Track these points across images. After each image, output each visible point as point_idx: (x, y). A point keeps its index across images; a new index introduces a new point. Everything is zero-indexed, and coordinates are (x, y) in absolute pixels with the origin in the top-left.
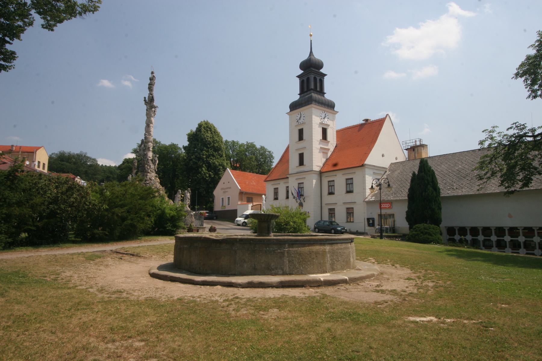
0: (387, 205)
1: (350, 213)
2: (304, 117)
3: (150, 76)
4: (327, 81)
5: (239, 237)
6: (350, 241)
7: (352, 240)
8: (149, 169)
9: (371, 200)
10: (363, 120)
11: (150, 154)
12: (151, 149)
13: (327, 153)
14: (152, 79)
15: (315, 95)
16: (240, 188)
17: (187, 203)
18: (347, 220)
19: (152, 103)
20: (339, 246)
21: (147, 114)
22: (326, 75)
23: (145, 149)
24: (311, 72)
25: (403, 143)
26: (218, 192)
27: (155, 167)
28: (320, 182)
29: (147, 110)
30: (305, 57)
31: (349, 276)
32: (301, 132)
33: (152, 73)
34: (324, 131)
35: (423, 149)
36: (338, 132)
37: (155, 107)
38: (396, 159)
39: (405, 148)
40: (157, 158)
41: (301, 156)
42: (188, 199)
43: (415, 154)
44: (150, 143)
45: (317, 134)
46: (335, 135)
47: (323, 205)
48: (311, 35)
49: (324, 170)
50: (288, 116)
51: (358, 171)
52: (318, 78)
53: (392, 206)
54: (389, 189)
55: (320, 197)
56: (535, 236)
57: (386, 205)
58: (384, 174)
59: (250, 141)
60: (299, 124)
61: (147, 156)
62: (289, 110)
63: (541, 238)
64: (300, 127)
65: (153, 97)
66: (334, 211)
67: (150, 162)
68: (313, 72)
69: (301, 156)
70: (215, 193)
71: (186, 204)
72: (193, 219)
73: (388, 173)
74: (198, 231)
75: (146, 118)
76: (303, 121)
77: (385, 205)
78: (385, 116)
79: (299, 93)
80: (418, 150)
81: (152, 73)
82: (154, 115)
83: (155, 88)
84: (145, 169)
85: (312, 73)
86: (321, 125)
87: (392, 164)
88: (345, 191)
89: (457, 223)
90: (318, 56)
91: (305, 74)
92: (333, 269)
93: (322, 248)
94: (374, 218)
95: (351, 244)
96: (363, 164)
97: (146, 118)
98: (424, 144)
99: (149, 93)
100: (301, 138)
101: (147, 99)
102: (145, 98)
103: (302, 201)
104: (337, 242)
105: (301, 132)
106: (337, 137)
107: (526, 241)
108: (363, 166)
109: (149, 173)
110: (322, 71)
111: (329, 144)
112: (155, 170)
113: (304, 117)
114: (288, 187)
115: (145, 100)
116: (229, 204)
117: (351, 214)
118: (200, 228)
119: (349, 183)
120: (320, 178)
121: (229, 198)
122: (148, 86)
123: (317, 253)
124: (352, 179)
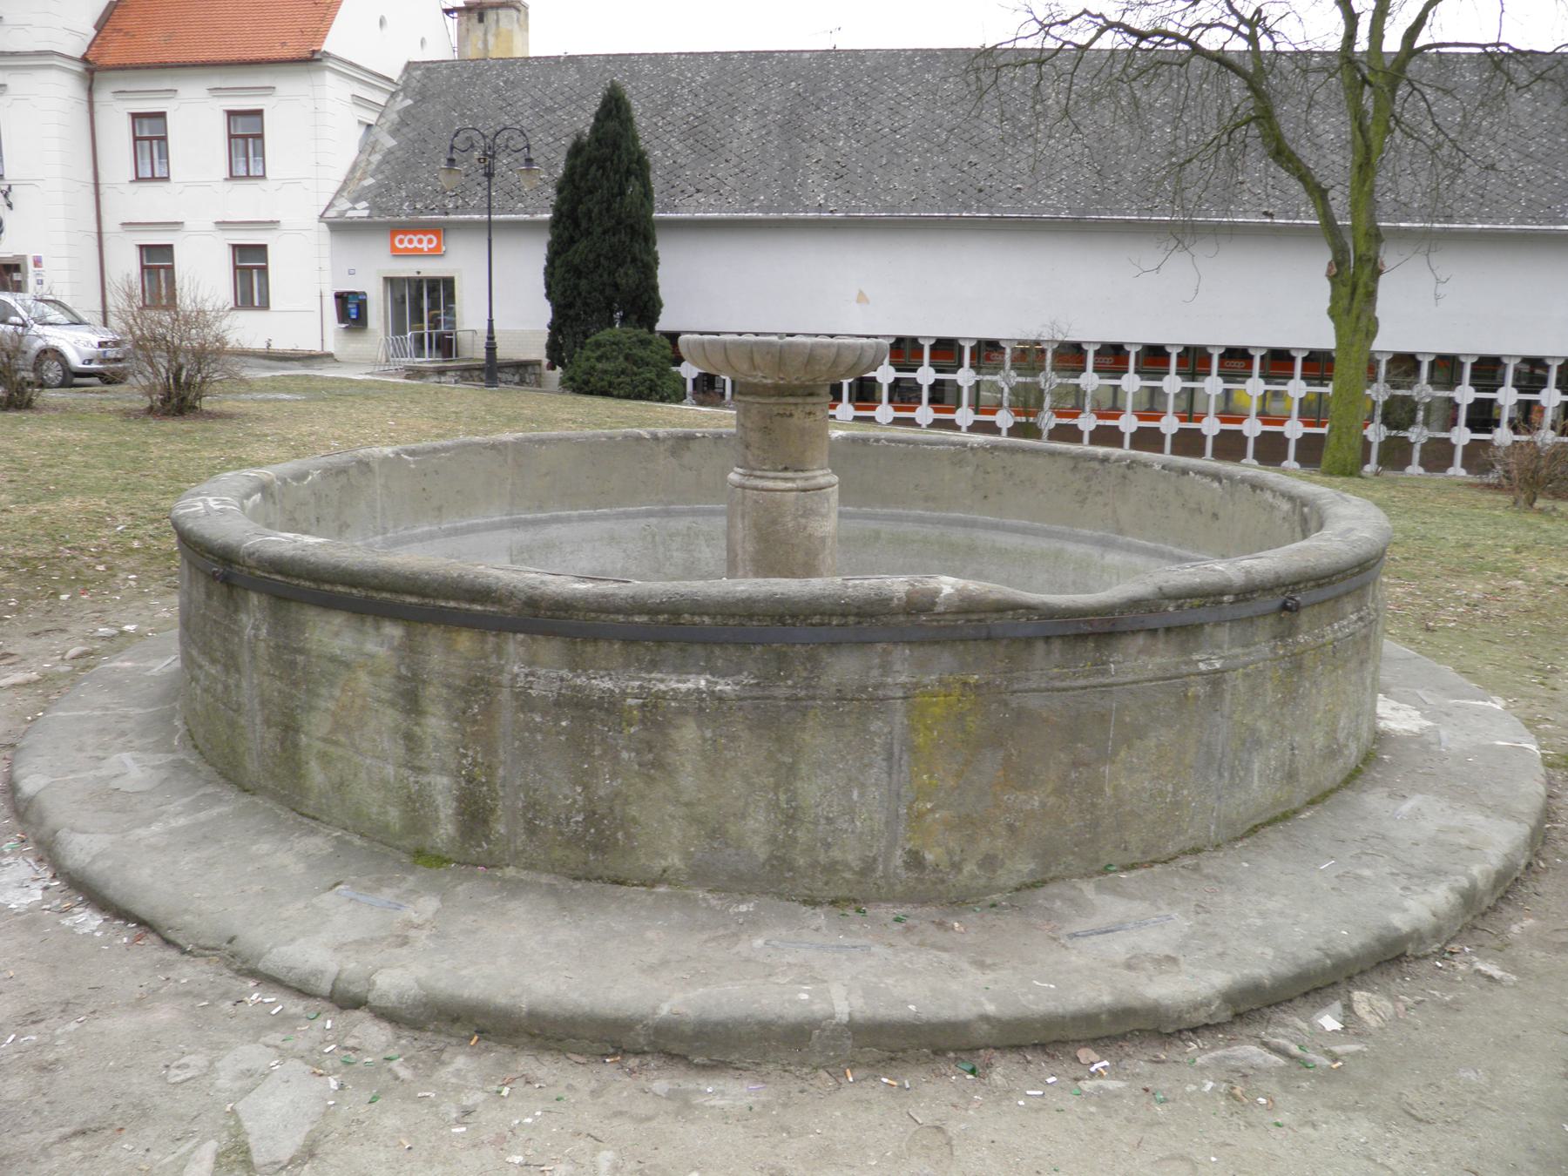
0: (425, 239)
9: (350, 214)
28: (85, 117)
43: (485, 34)
47: (105, 229)
55: (92, 188)
56: (1126, 371)
57: (420, 241)
63: (1564, 393)
66: (171, 258)
77: (415, 239)
80: (498, 21)
89: (1427, 342)
94: (364, 294)
96: (314, 52)
107: (897, 380)
117: (162, 272)
124: (258, 113)
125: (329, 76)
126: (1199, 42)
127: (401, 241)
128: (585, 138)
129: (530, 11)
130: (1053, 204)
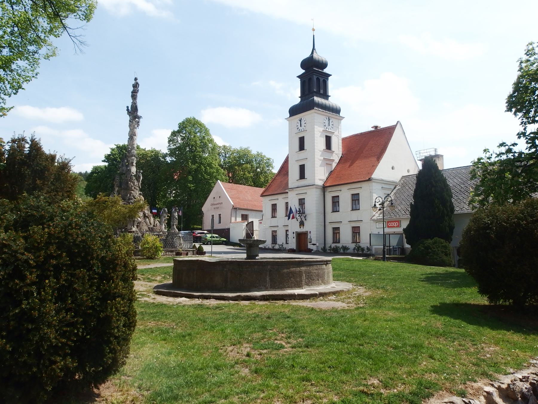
0: (395, 223)
1: (357, 232)
2: (305, 123)
3: (134, 82)
4: (331, 83)
5: (230, 260)
6: (326, 263)
7: (326, 263)
8: (133, 186)
10: (372, 127)
11: (134, 169)
12: (134, 164)
13: (331, 165)
14: (136, 86)
15: (317, 99)
16: (233, 204)
17: (175, 224)
18: (391, 234)
19: (136, 113)
20: (315, 267)
21: (130, 126)
22: (330, 75)
23: (128, 164)
24: (313, 73)
25: (417, 153)
26: (207, 208)
27: (139, 184)
29: (130, 121)
30: (307, 55)
31: (319, 292)
32: (302, 140)
33: (136, 79)
34: (328, 140)
35: (439, 160)
36: (344, 140)
37: (139, 118)
38: (408, 171)
39: (419, 159)
40: (141, 174)
41: (302, 168)
42: (176, 218)
44: (133, 157)
45: (321, 144)
46: (341, 144)
48: (314, 30)
49: (328, 185)
50: (287, 122)
51: (365, 185)
52: (321, 80)
53: (400, 225)
54: (393, 208)
55: (323, 214)
58: (394, 188)
59: (244, 146)
60: (300, 131)
61: (131, 171)
62: (289, 115)
64: (301, 136)
65: (136, 106)
67: (134, 178)
68: (315, 73)
69: (302, 168)
70: (204, 209)
71: (173, 225)
72: (182, 241)
73: (398, 187)
74: (187, 255)
75: (128, 129)
76: (304, 128)
77: (393, 223)
78: (395, 124)
79: (300, 96)
81: (136, 79)
82: (138, 126)
83: (140, 96)
84: (128, 186)
85: (314, 74)
86: (324, 133)
87: (403, 177)
88: (350, 208)
90: (320, 55)
91: (307, 74)
92: (308, 284)
93: (298, 269)
95: (326, 266)
96: (369, 178)
97: (129, 130)
98: (439, 155)
99: (132, 101)
100: (302, 147)
101: (130, 108)
102: (128, 107)
103: (303, 219)
104: (312, 264)
105: (302, 140)
106: (343, 146)
108: (370, 180)
109: (132, 190)
110: (326, 71)
111: (334, 154)
112: (139, 187)
113: (305, 123)
114: (287, 203)
115: (128, 110)
116: (220, 222)
118: (190, 250)
119: (355, 198)
120: (323, 193)
121: (220, 215)
122: (131, 94)
123: (293, 273)
125: (374, 183)
126: (215, 228)
127: (390, 224)
128: (413, 203)
129: (181, 121)
130: (469, 167)
